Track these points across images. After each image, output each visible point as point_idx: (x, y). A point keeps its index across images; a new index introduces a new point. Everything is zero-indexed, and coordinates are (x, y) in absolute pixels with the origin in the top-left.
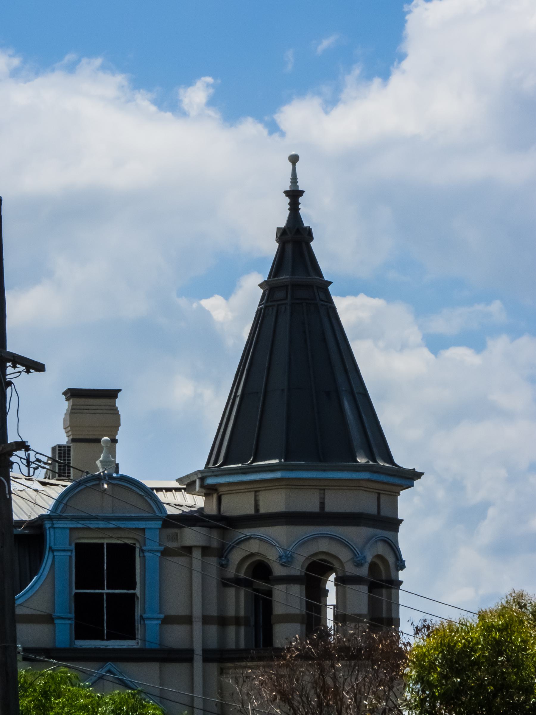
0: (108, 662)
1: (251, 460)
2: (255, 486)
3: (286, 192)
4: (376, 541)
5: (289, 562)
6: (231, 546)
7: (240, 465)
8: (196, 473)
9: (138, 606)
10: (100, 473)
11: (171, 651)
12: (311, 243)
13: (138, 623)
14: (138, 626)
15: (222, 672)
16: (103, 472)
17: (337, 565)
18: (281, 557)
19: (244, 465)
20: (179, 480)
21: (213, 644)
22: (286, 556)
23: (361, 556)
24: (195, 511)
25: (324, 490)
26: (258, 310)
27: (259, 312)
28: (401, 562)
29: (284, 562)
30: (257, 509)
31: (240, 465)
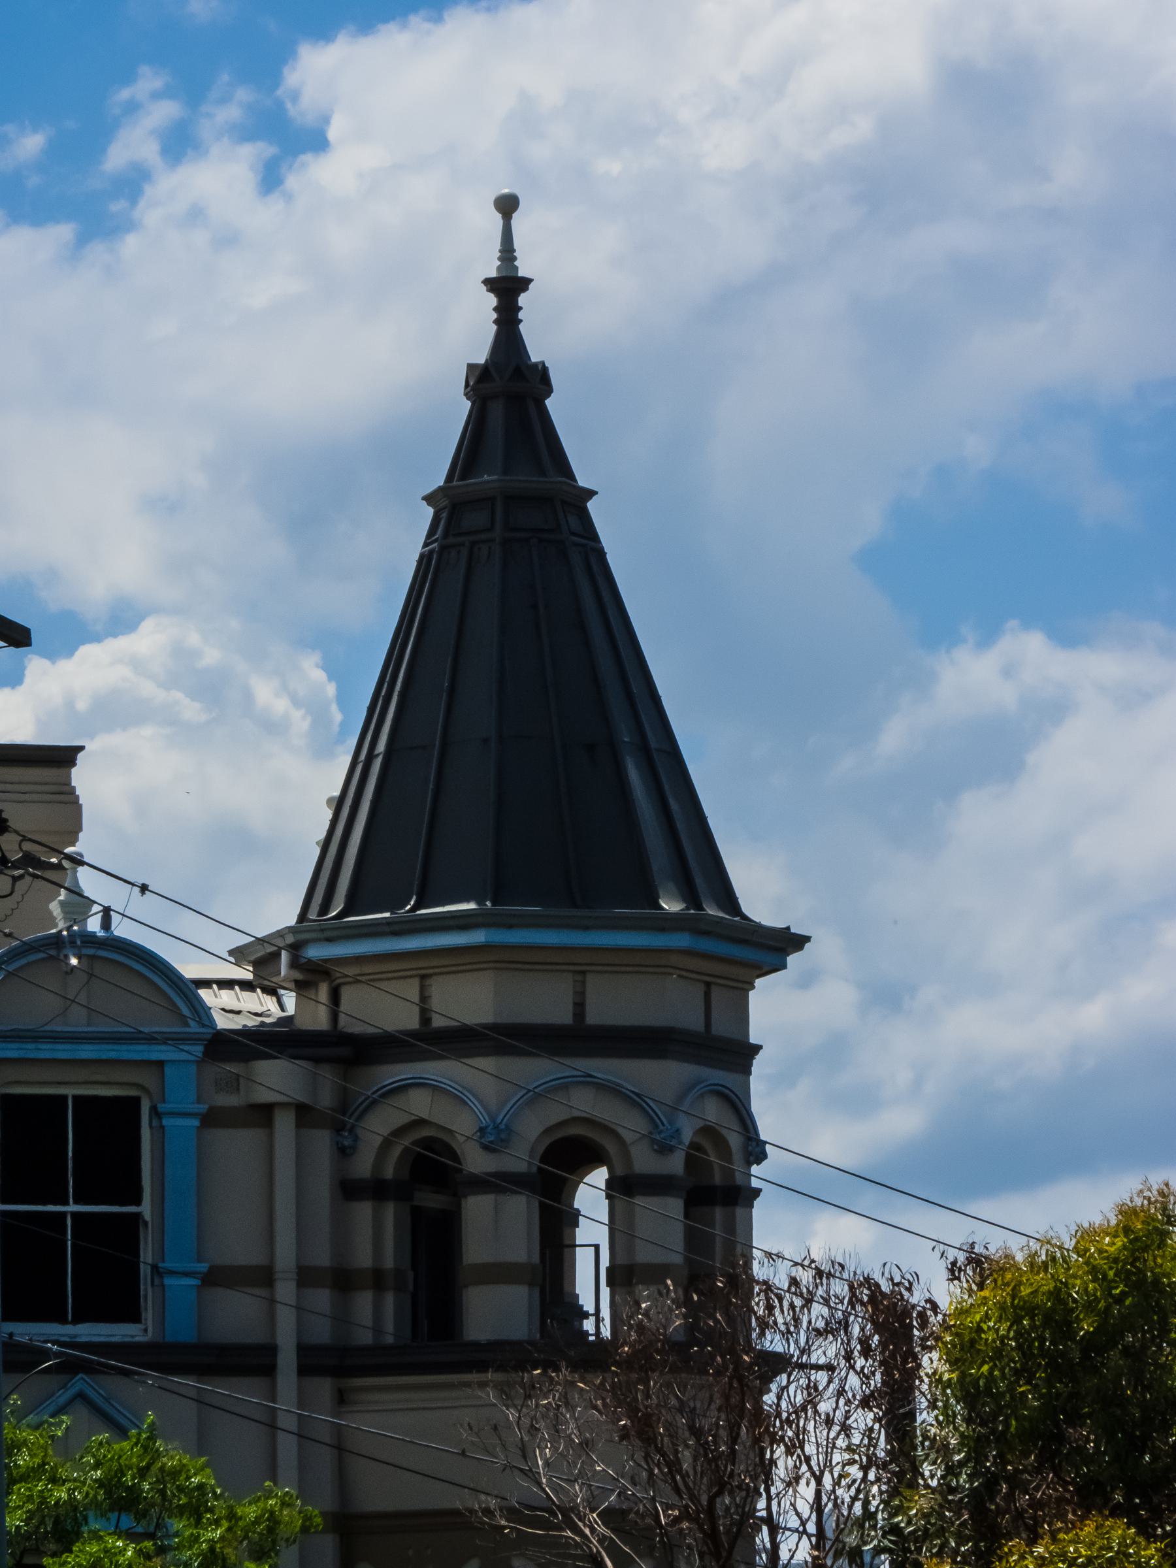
0: (76, 1374)
1: (412, 903)
2: (421, 964)
3: (487, 282)
4: (702, 1095)
5: (502, 1141)
6: (371, 1099)
7: (387, 915)
8: (281, 934)
9: (146, 1243)
10: (61, 931)
11: (223, 1350)
12: (547, 402)
13: (145, 1284)
14: (146, 1290)
15: (342, 1399)
16: (69, 928)
17: (611, 1148)
18: (482, 1130)
19: (397, 914)
20: (239, 955)
21: (322, 1332)
22: (496, 1127)
23: (669, 1127)
24: (272, 1024)
25: (584, 973)
26: (422, 556)
27: (424, 561)
28: (758, 1145)
29: (491, 1142)
30: (425, 1019)
31: (387, 915)
